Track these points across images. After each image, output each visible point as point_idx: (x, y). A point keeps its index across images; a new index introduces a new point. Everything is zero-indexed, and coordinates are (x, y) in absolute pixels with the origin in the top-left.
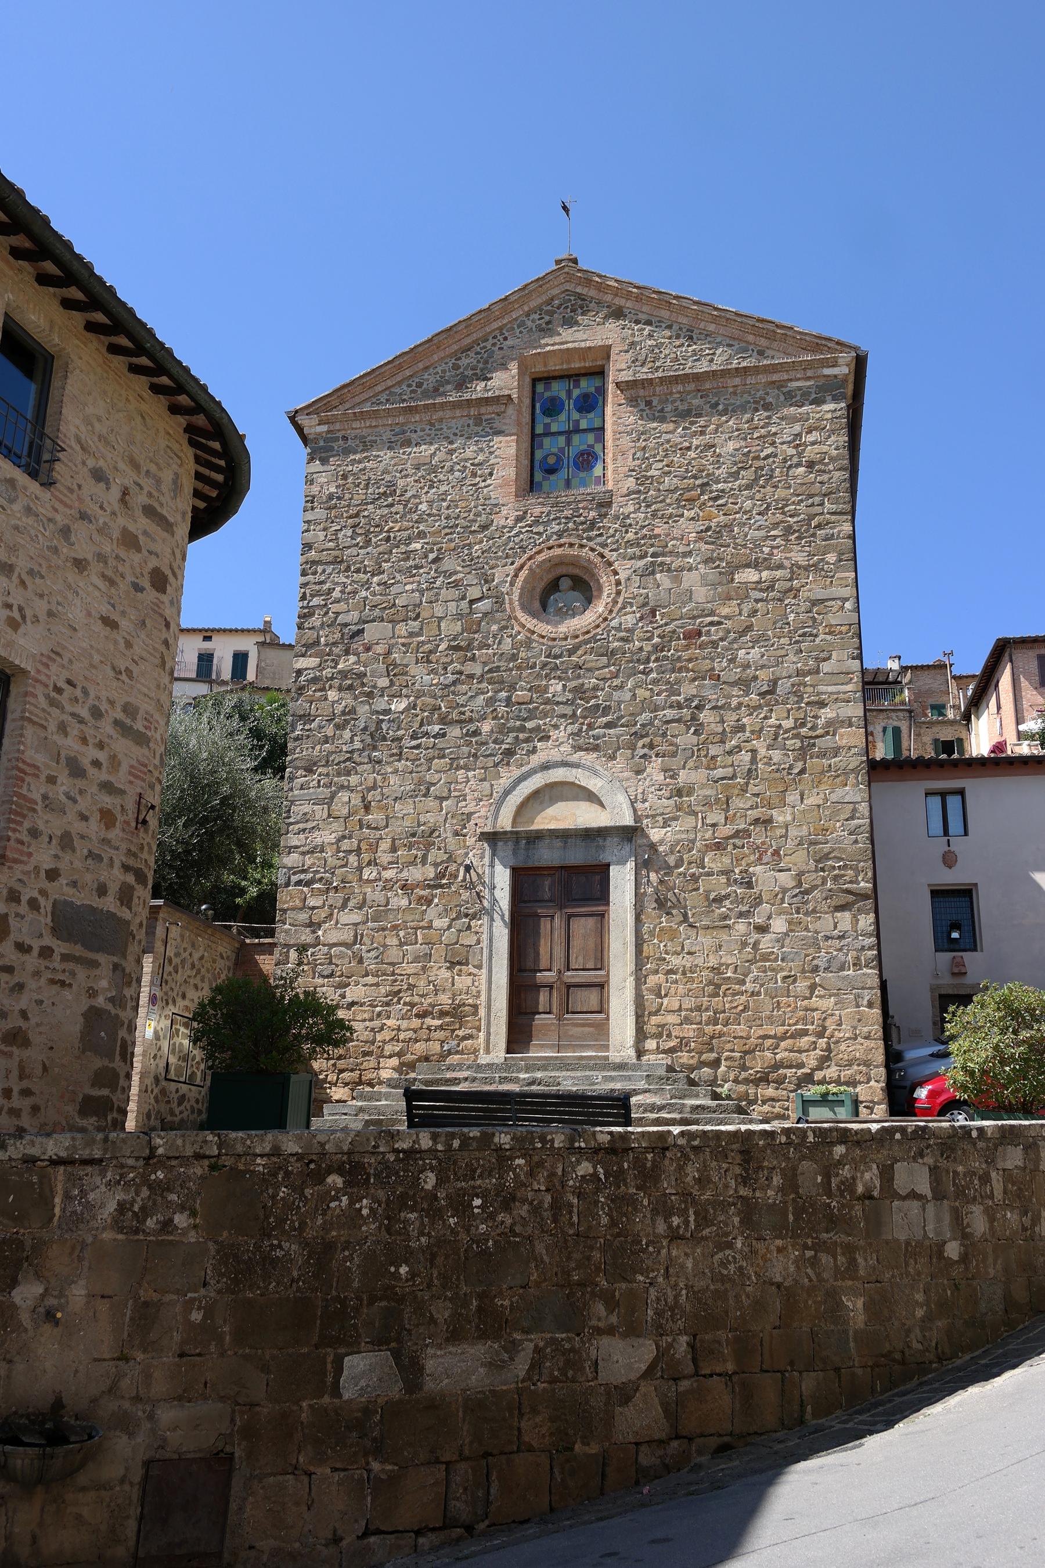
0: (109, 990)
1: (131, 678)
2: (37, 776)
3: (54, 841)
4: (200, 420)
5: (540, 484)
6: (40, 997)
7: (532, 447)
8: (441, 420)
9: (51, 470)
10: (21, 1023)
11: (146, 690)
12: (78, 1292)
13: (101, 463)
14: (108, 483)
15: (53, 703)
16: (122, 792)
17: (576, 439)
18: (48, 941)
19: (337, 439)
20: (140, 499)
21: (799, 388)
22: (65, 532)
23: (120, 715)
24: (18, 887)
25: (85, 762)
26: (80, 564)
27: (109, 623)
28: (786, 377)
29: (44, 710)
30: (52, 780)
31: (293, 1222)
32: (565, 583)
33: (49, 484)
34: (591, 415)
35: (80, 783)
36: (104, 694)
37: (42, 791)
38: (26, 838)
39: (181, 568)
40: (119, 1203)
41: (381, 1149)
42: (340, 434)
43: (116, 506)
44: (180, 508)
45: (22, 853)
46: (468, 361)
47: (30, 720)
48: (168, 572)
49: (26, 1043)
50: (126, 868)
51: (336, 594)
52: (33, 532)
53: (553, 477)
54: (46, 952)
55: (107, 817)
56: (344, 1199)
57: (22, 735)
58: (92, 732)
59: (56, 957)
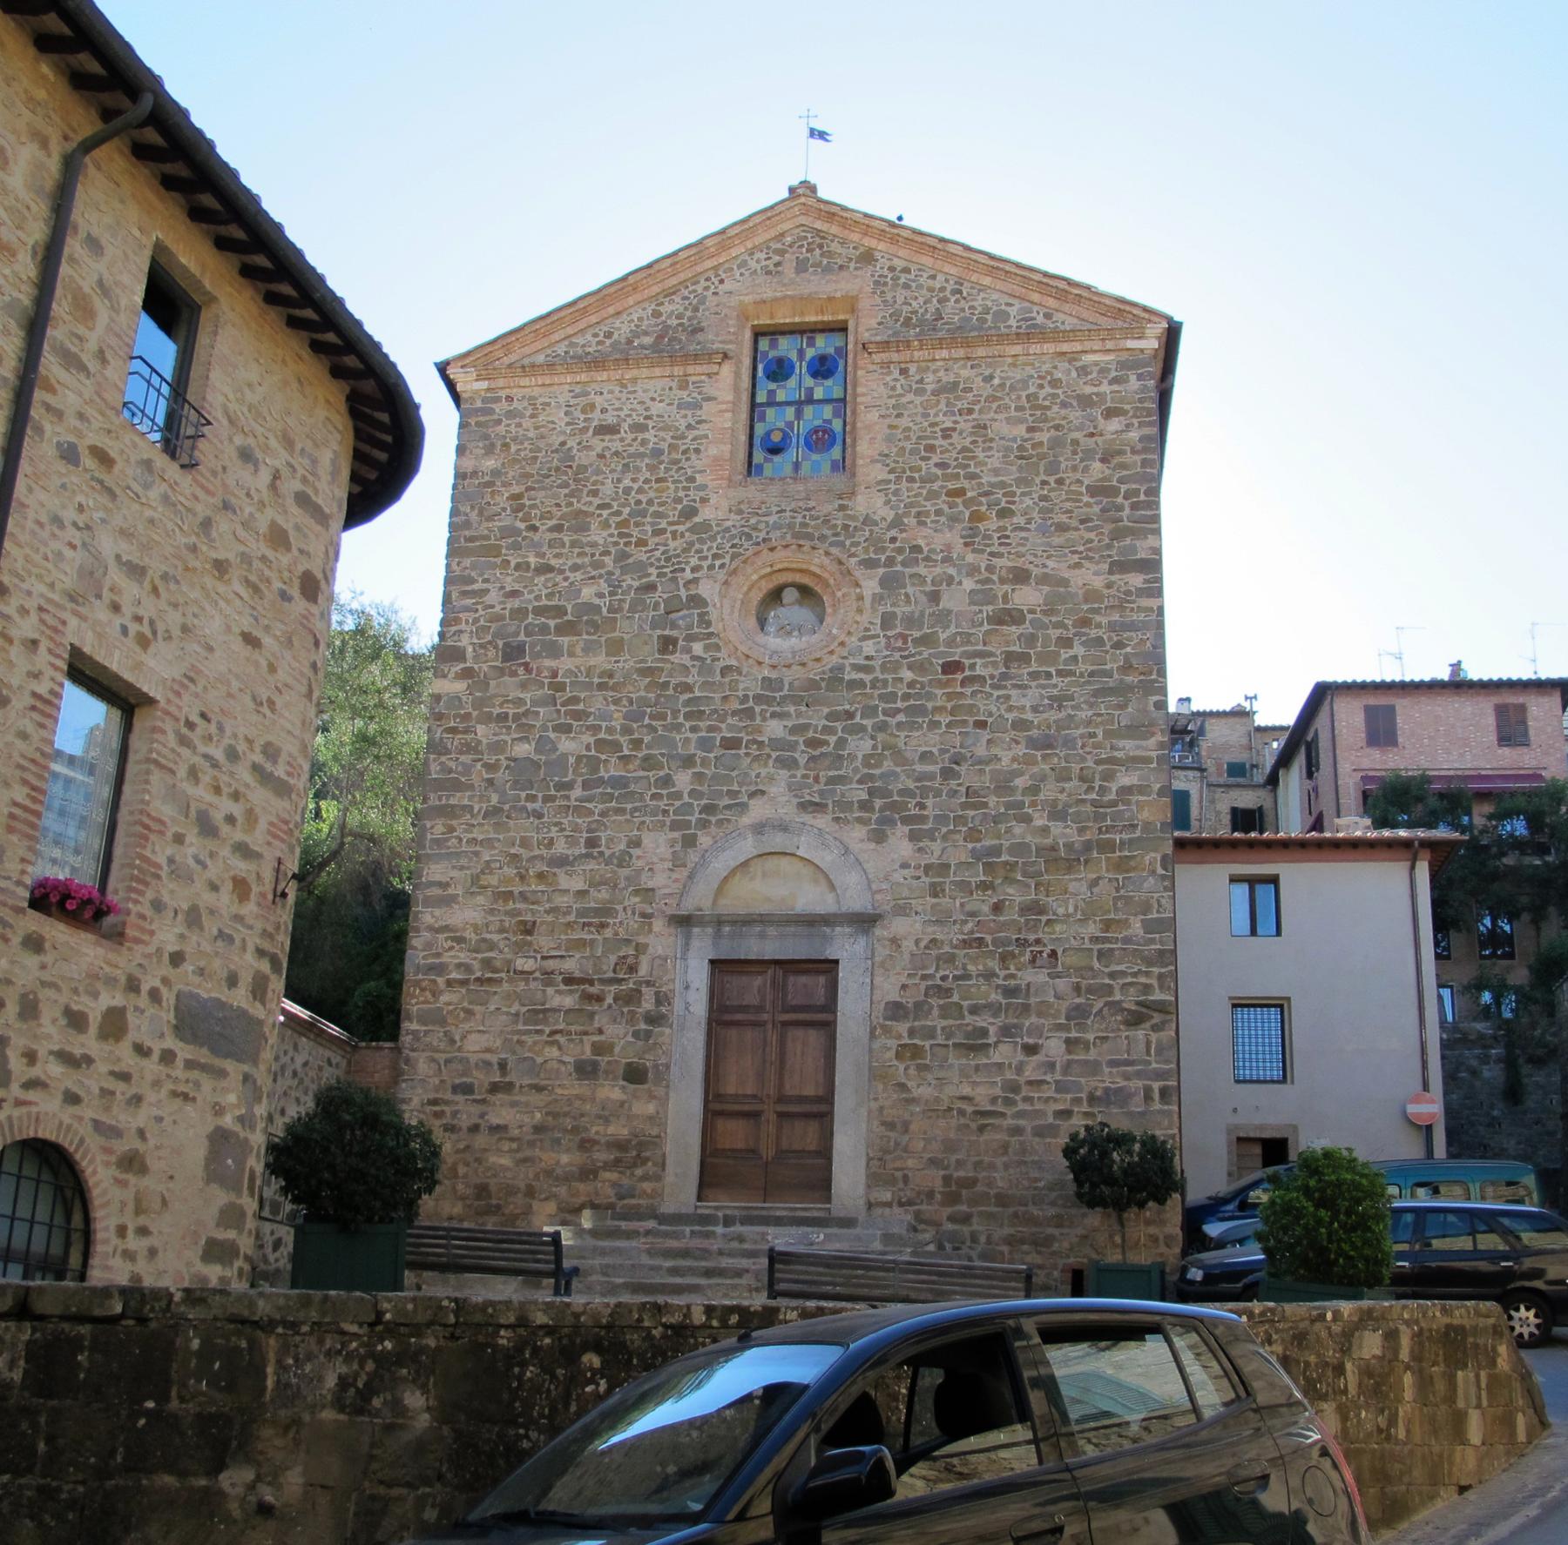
0: (238, 1106)
1: (273, 711)
2: (161, 833)
3: (180, 916)
4: (368, 386)
5: (760, 468)
6: (160, 1113)
7: (752, 420)
8: (634, 380)
9: (193, 448)
10: (137, 1144)
11: (289, 726)
12: (294, 1480)
13: (251, 441)
14: (256, 464)
15: (184, 741)
16: (259, 856)
17: (809, 411)
18: (170, 1042)
19: (498, 400)
20: (291, 486)
21: (1096, 364)
22: (207, 524)
23: (258, 758)
24: (137, 973)
25: (218, 817)
26: (221, 567)
27: (250, 640)
28: (1079, 348)
29: (173, 750)
30: (179, 839)
31: (542, 1408)
32: (790, 595)
33: (190, 466)
34: (829, 382)
35: (211, 844)
36: (242, 731)
37: (169, 852)
38: (149, 912)
39: (333, 570)
40: (340, 1377)
41: (646, 1324)
42: (503, 394)
43: (266, 494)
44: (334, 493)
45: (143, 930)
46: (671, 308)
47: (156, 762)
48: (320, 576)
49: (143, 1170)
50: (261, 953)
52: (170, 525)
53: (777, 459)
54: (168, 1057)
55: (241, 887)
56: (603, 1382)
57: (147, 782)
58: (226, 778)
59: (179, 1063)
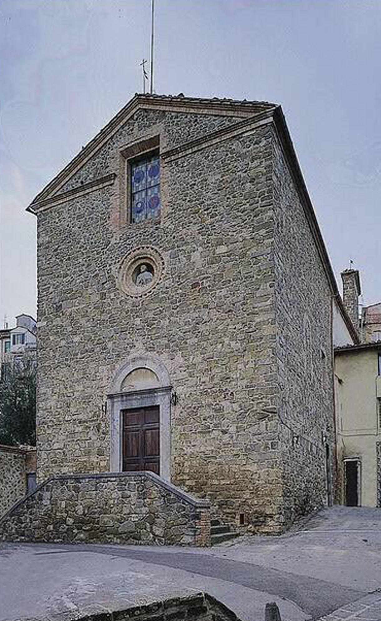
51: (51, 290)
